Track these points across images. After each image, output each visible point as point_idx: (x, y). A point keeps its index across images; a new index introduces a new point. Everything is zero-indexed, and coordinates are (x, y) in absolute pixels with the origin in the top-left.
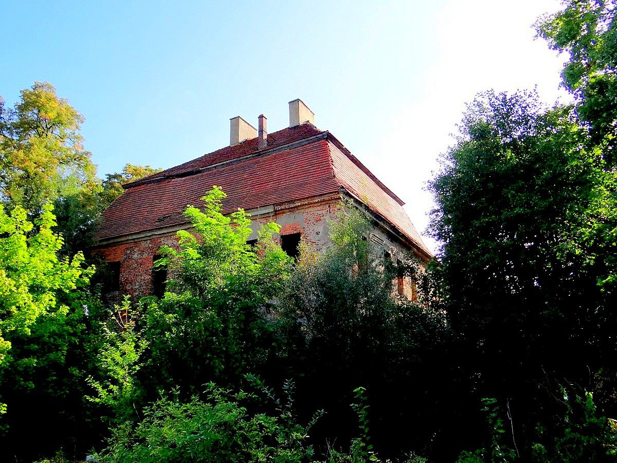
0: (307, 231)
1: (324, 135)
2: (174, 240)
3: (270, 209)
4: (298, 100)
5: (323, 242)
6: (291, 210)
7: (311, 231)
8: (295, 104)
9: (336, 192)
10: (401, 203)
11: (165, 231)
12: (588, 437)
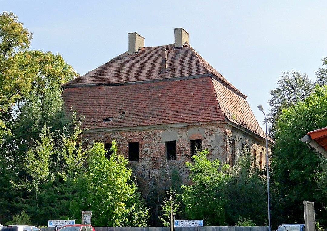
0: (206, 139)
1: (209, 75)
2: (119, 135)
3: (185, 125)
4: (181, 29)
5: (215, 146)
6: (197, 126)
7: (208, 139)
8: (178, 32)
9: (223, 120)
10: (245, 97)
11: (114, 130)
12: (202, 221)
